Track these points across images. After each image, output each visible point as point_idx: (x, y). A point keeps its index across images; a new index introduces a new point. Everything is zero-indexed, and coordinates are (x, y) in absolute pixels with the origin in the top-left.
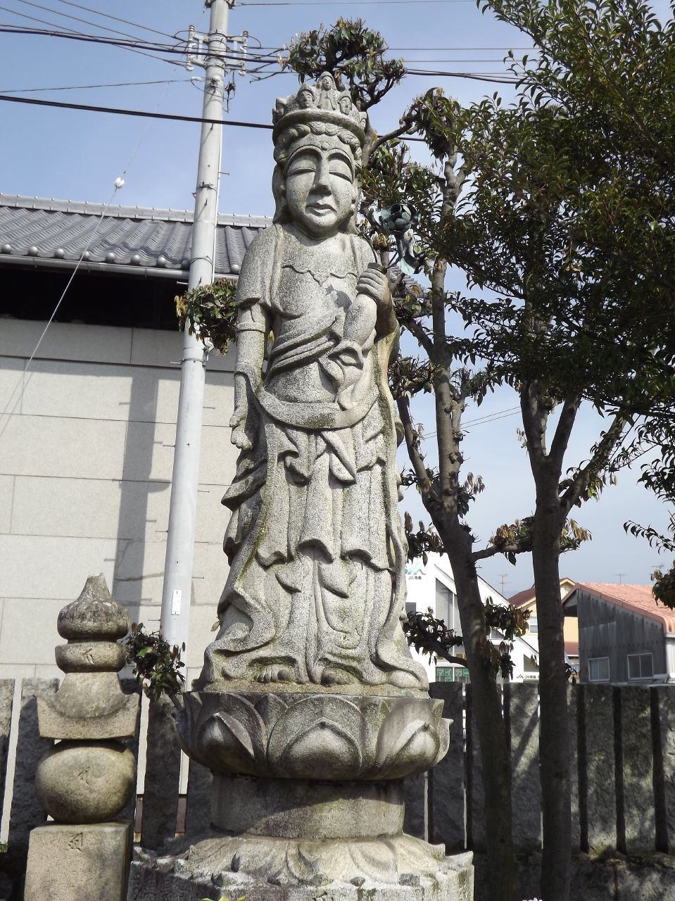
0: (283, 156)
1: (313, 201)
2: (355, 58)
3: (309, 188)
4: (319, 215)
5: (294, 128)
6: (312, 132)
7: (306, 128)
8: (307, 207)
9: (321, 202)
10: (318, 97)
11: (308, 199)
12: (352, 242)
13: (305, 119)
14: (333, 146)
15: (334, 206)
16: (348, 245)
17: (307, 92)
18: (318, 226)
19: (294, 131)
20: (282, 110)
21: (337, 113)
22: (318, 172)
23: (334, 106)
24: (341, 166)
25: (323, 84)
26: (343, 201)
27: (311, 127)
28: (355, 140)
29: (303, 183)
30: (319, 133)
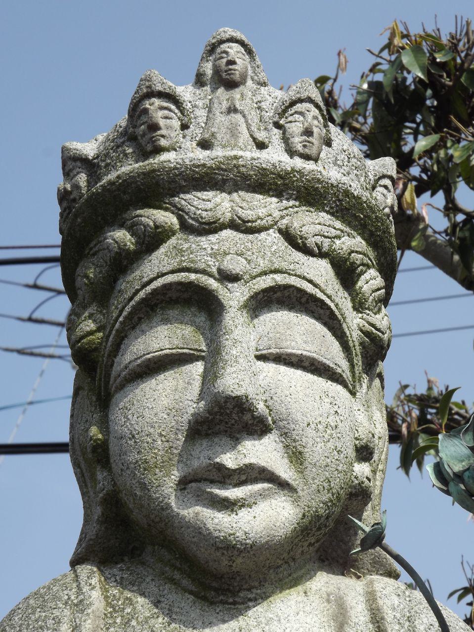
0: (90, 325)
1: (200, 458)
2: (370, 120)
3: (187, 417)
4: (228, 505)
5: (122, 226)
6: (185, 227)
7: (166, 218)
8: (183, 484)
9: (230, 460)
10: (201, 114)
11: (184, 457)
12: (371, 598)
13: (159, 189)
14: (263, 264)
15: (285, 471)
16: (359, 613)
17: (157, 102)
18: (227, 547)
19: (121, 236)
20: (82, 179)
21: (275, 156)
22: (213, 358)
23: (261, 136)
24: (301, 332)
25: (217, 71)
26: (317, 450)
27: (180, 212)
28: (352, 243)
29: (162, 405)
30: (210, 228)
